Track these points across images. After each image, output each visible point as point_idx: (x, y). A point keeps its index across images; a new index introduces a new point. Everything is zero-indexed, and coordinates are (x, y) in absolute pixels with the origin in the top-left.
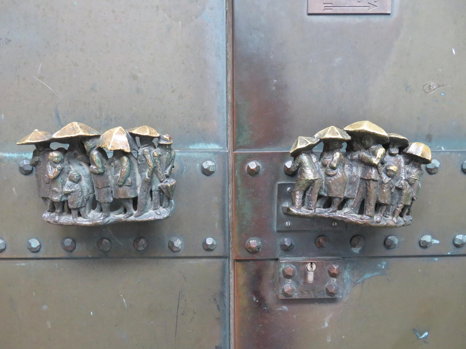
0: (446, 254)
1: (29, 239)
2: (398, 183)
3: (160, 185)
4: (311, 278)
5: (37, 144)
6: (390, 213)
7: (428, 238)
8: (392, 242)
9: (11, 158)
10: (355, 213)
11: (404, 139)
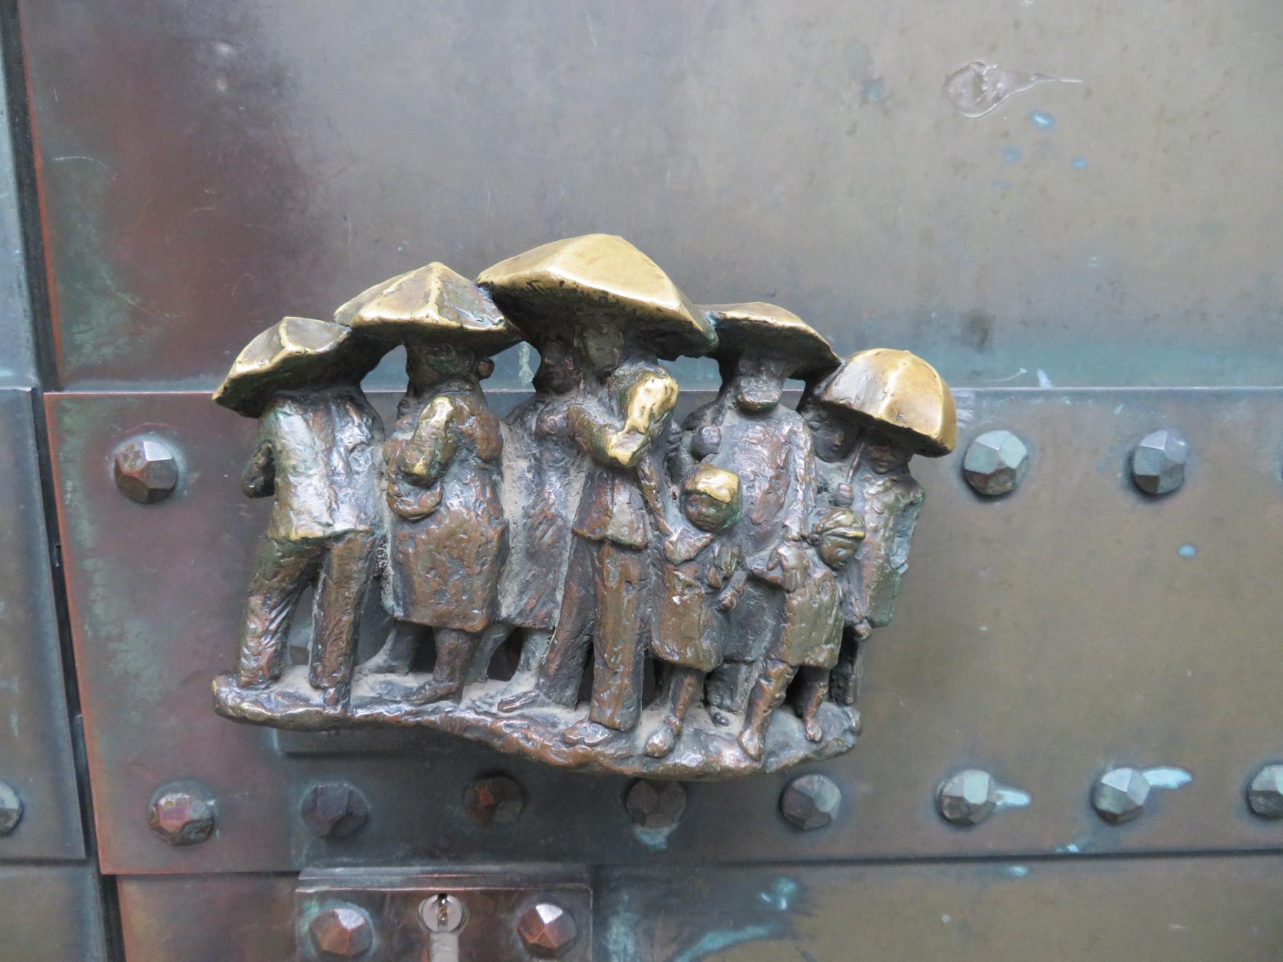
0: (1059, 850)
2: (765, 554)
6: (741, 701)
7: (974, 787)
8: (810, 802)
10: (559, 703)
11: (794, 331)
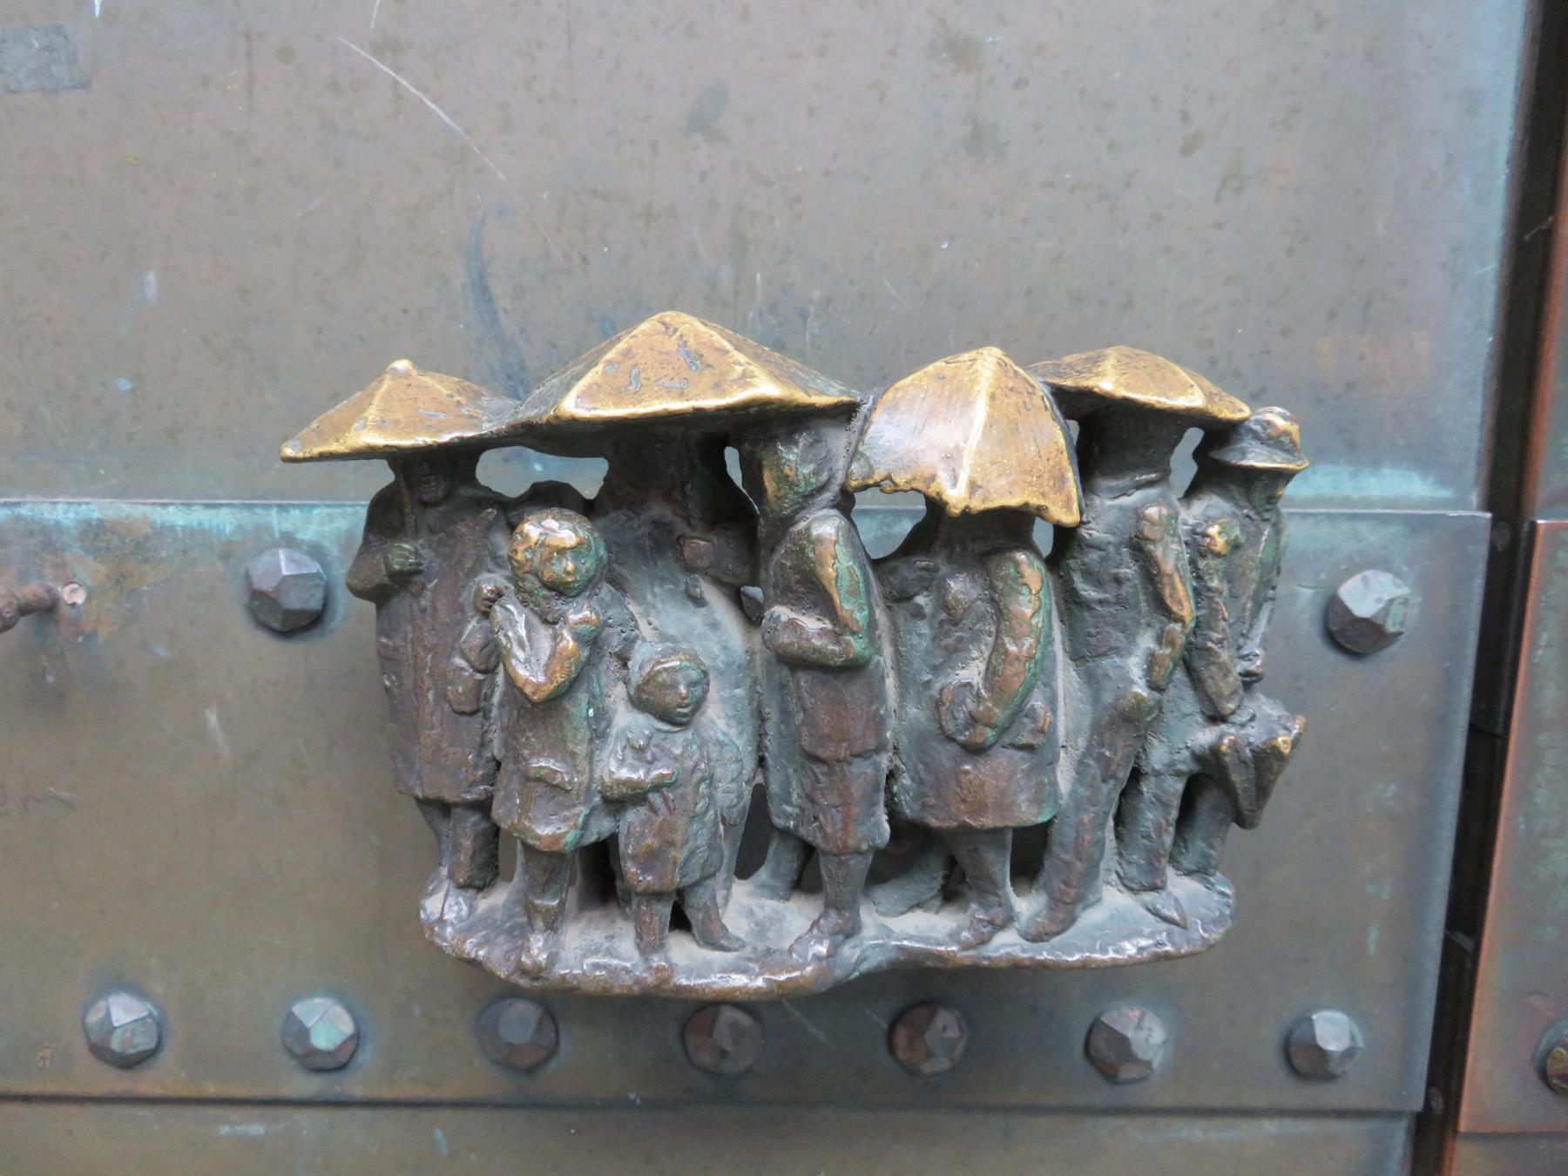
1: (298, 998)
3: (1204, 737)
5: (401, 460)
9: (197, 535)
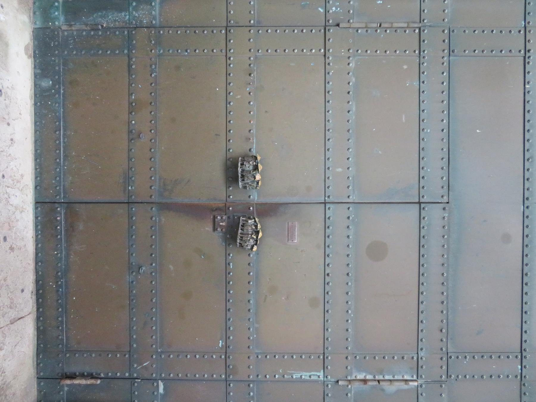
4: (221, 224)
7: (231, 255)
